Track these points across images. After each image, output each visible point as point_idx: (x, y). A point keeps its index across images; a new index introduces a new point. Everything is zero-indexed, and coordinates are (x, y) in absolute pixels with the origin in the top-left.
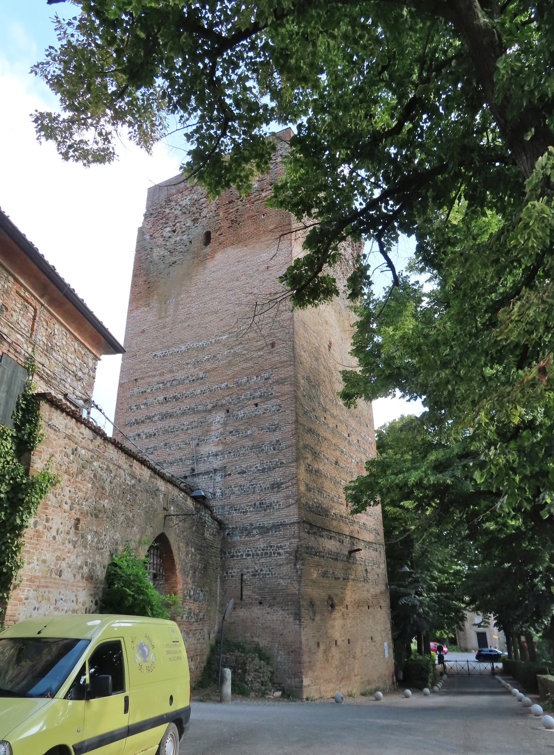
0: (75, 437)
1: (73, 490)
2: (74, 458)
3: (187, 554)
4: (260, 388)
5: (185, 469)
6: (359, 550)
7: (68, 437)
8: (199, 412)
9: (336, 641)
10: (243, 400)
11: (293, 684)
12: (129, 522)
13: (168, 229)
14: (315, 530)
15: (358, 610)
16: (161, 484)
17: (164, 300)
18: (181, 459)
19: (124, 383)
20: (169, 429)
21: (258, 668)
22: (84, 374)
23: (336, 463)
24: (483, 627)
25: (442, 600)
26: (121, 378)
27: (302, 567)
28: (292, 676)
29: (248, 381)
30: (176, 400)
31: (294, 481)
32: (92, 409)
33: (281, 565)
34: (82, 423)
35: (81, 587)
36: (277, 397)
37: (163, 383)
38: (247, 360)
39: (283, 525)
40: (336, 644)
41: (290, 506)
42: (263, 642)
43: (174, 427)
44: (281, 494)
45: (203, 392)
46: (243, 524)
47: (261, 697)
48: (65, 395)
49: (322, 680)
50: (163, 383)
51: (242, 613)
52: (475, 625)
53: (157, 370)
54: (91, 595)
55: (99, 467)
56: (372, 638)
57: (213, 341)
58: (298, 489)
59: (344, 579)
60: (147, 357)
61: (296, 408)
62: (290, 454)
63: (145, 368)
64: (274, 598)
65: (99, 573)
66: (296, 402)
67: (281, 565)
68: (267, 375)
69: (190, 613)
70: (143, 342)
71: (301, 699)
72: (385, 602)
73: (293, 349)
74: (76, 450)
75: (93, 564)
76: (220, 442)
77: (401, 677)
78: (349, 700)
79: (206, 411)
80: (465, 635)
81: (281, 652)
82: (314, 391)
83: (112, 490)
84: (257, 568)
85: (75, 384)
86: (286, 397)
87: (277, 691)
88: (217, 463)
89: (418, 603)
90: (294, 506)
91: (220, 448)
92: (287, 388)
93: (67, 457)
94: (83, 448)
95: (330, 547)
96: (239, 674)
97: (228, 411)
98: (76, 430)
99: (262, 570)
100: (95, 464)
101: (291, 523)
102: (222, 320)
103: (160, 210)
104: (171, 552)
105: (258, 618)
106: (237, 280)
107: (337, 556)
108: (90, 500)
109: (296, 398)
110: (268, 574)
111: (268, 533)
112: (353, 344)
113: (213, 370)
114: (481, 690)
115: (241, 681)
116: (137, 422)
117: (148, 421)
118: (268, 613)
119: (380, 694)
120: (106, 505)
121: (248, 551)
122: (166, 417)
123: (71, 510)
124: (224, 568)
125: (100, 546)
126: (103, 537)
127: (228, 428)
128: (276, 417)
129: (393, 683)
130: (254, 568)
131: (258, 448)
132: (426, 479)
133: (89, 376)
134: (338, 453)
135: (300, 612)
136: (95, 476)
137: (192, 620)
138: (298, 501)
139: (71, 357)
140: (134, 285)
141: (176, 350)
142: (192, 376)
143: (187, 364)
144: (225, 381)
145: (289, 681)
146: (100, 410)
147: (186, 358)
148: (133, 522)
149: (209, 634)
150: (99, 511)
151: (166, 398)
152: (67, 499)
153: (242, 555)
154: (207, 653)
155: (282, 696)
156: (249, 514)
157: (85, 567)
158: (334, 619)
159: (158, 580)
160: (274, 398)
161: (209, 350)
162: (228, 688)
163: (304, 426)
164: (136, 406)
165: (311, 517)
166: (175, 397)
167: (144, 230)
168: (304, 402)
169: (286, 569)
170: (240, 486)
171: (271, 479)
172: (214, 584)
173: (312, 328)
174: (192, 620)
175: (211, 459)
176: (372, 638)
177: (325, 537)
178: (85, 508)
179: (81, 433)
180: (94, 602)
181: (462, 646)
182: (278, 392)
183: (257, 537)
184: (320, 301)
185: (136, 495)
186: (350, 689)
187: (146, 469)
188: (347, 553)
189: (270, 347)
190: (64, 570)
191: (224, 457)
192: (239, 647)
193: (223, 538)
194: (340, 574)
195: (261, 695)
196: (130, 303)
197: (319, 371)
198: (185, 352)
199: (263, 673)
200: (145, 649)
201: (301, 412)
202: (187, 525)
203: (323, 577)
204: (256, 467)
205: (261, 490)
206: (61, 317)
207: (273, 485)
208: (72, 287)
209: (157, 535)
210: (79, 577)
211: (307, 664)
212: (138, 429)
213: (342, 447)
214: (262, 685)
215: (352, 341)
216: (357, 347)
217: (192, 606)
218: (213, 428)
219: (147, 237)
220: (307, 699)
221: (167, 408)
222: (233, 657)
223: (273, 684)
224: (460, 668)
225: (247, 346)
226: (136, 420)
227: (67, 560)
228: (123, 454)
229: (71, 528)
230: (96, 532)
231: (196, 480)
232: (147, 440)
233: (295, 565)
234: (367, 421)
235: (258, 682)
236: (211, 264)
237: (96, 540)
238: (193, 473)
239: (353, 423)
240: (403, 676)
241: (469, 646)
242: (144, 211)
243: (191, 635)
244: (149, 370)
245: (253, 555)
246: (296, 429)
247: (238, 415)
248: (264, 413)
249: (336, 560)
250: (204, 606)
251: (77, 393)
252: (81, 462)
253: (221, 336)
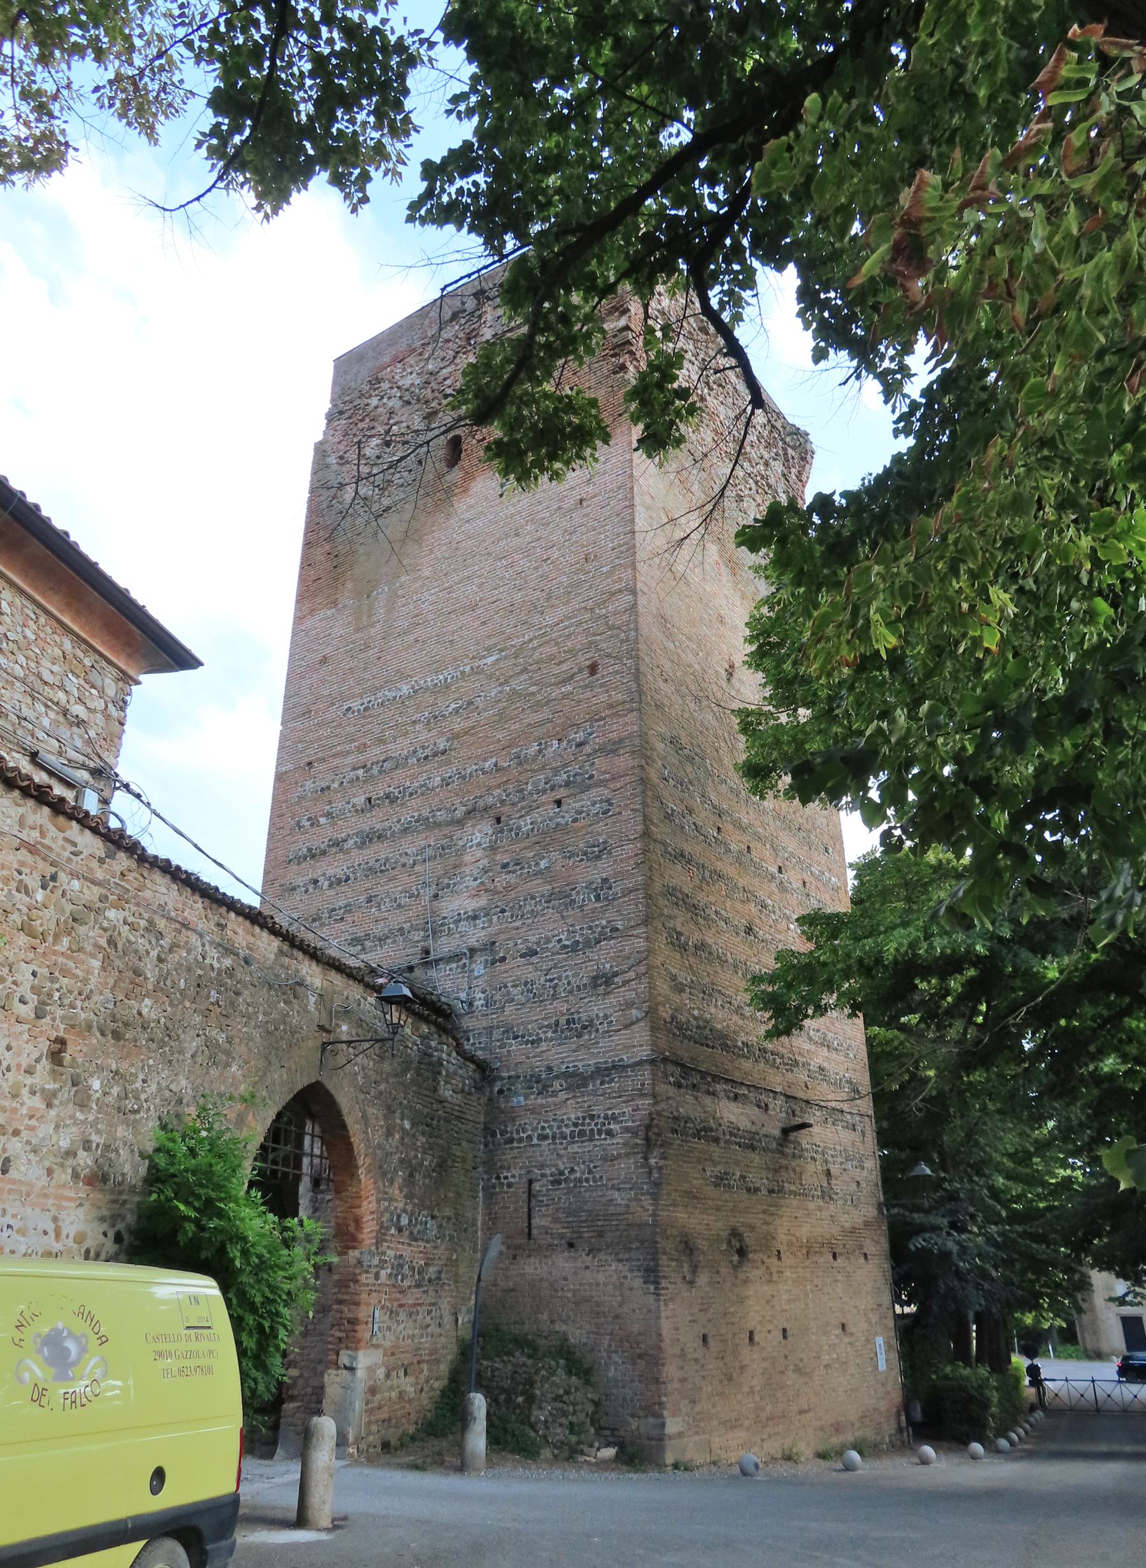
0: (50, 848)
1: (45, 971)
2: (46, 897)
3: (389, 1133)
4: (565, 765)
5: (409, 951)
6: (804, 1126)
7: (32, 849)
8: (438, 825)
9: (751, 1333)
10: (531, 794)
11: (642, 1429)
12: (216, 1055)
13: (375, 441)
14: (695, 1079)
15: (807, 1263)
16: (312, 973)
17: (366, 592)
18: (401, 929)
19: (286, 772)
20: (377, 865)
21: (561, 1392)
22: (91, 710)
23: (749, 930)
24: (1131, 1304)
25: (1014, 1241)
26: (280, 761)
27: (662, 1163)
28: (641, 1413)
29: (540, 751)
30: (391, 802)
31: (642, 969)
32: (117, 793)
33: (614, 1159)
34: (71, 817)
35: (70, 1199)
36: (602, 783)
37: (364, 766)
38: (538, 706)
39: (618, 1067)
40: (751, 1339)
41: (632, 1024)
42: (577, 1335)
43: (387, 859)
44: (612, 1000)
45: (446, 782)
46: (532, 1068)
47: (567, 1460)
48: (34, 756)
49: (715, 1423)
50: (364, 766)
51: (531, 1268)
52: (1111, 1299)
53: (353, 741)
54: (102, 1219)
55: (125, 923)
56: (843, 1326)
57: (468, 669)
58: (651, 987)
59: (771, 1191)
60: (333, 713)
61: (644, 804)
62: (630, 910)
63: (327, 738)
64: (601, 1234)
65: (127, 1169)
66: (644, 792)
67: (614, 1159)
68: (580, 736)
69: (401, 1266)
70: (323, 681)
71: (660, 1465)
72: (877, 1245)
73: (637, 675)
74: (54, 878)
75: (107, 1147)
76: (483, 889)
77: (918, 1415)
78: (783, 1469)
79: (452, 822)
80: (1094, 1322)
81: (616, 1358)
82: (689, 769)
83: (162, 978)
84: (562, 1167)
85: (65, 732)
86: (623, 781)
87: (607, 1445)
88: (475, 935)
89: (955, 1249)
90: (642, 1024)
91: (483, 902)
92: (624, 761)
93: (27, 893)
94: (74, 875)
95: (733, 1119)
96: (518, 1406)
97: (498, 820)
98: (52, 831)
99: (572, 1171)
100: (112, 914)
101: (637, 1064)
102: (484, 623)
103: (358, 402)
104: (343, 1126)
105: (566, 1279)
106: (517, 535)
107: (752, 1138)
108: (96, 998)
109: (644, 781)
110: (587, 1180)
111: (585, 1085)
112: (750, 640)
113: (466, 733)
114: (1115, 1448)
115: (522, 1423)
116: (312, 855)
117: (334, 850)
118: (587, 1268)
119: (854, 1455)
120: (145, 1011)
121: (543, 1128)
122: (371, 840)
123: (38, 1017)
124: (492, 1167)
125: (130, 1104)
126: (138, 1085)
127: (498, 857)
128: (600, 827)
129: (900, 1430)
130: (556, 1165)
131: (562, 898)
132: (925, 945)
133: (108, 717)
134: (753, 908)
135: (657, 1265)
136: (111, 942)
137: (407, 1283)
138: (651, 1013)
139: (49, 670)
140: (307, 563)
141: (390, 695)
142: (423, 747)
143: (414, 722)
144: (492, 754)
145: (634, 1424)
146: (138, 796)
147: (411, 711)
148: (228, 1053)
149: (455, 1315)
150: (126, 1024)
151: (369, 800)
152: (25, 990)
153: (530, 1137)
154: (450, 1357)
155: (617, 1458)
156: (544, 1046)
157: (82, 1154)
158: (746, 1281)
159: (323, 1192)
160: (596, 785)
161: (458, 689)
162: (477, 1439)
163: (665, 844)
164: (309, 819)
165: (685, 1050)
166: (388, 796)
167: (326, 447)
168: (666, 794)
169: (627, 1167)
170: (526, 984)
171: (592, 967)
172: (468, 1203)
173: (686, 631)
174: (407, 1283)
175: (464, 926)
176: (843, 1326)
177: (722, 1094)
178: (83, 1016)
179: (66, 840)
180: (111, 1234)
181: (1089, 1346)
182: (605, 772)
183: (563, 1096)
184: (567, 463)
185: (238, 994)
186: (788, 1443)
187: (265, 934)
188: (777, 1133)
189: (586, 673)
190: (17, 1157)
191: (490, 921)
192: (523, 1343)
193: (490, 1099)
194: (760, 1179)
195: (566, 1454)
196: (297, 602)
197: (702, 725)
198: (409, 697)
199: (574, 1404)
200: (71, 1345)
201: (655, 814)
202: (386, 1067)
203: (716, 1185)
204: (560, 941)
205: (571, 992)
206: (18, 574)
207: (595, 978)
208: (31, 499)
209: (299, 1087)
210: (65, 1176)
211: (676, 1385)
212: (314, 868)
213: (762, 895)
214: (572, 1432)
215: (747, 632)
216: (760, 646)
217: (406, 1251)
218: (467, 858)
219: (333, 460)
220: (676, 1466)
221: (374, 821)
222: (510, 1367)
223: (599, 1429)
224: (1075, 1395)
225: (537, 676)
226: (310, 850)
227: (25, 1134)
228: (197, 897)
229: (37, 1061)
230: (117, 1073)
231: (433, 973)
232: (332, 892)
233: (646, 1158)
234: (826, 840)
235: (561, 1425)
236: (462, 505)
237: (115, 1090)
238: (428, 960)
239: (790, 843)
240: (924, 1411)
241: (1105, 1347)
242: (326, 406)
243: (402, 1316)
244: (335, 741)
245: (554, 1138)
246: (645, 851)
247: (519, 828)
248: (575, 820)
249: (753, 1148)
250: (439, 1252)
251: (72, 754)
252: (69, 908)
253: (484, 657)
